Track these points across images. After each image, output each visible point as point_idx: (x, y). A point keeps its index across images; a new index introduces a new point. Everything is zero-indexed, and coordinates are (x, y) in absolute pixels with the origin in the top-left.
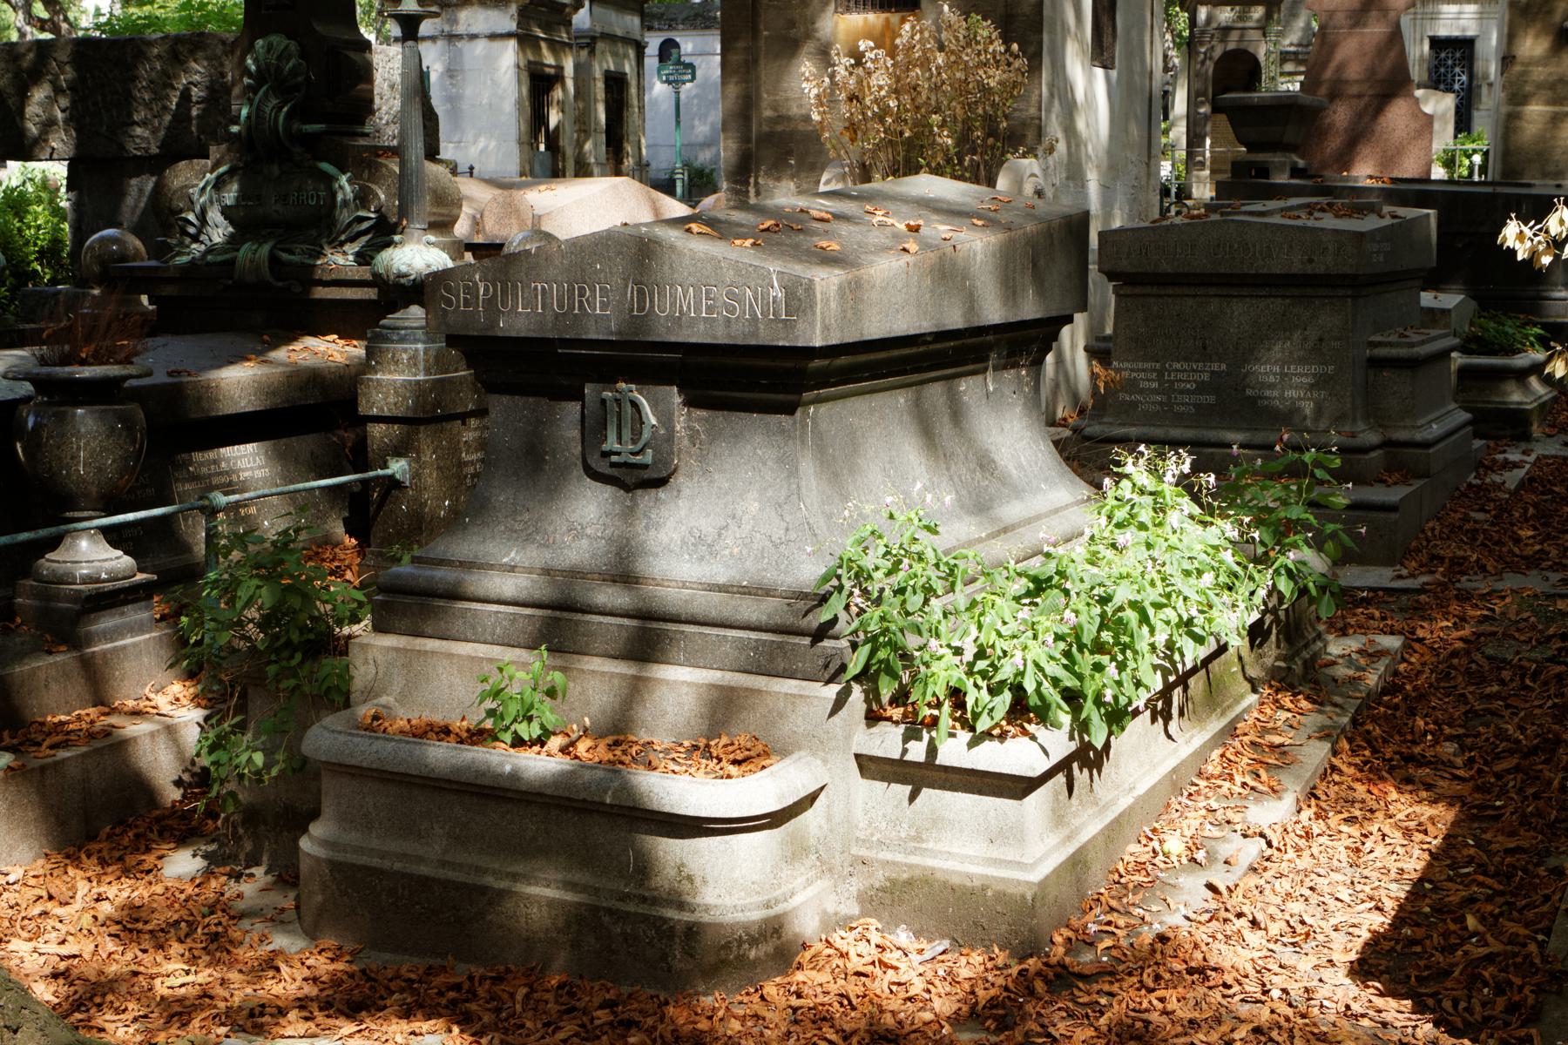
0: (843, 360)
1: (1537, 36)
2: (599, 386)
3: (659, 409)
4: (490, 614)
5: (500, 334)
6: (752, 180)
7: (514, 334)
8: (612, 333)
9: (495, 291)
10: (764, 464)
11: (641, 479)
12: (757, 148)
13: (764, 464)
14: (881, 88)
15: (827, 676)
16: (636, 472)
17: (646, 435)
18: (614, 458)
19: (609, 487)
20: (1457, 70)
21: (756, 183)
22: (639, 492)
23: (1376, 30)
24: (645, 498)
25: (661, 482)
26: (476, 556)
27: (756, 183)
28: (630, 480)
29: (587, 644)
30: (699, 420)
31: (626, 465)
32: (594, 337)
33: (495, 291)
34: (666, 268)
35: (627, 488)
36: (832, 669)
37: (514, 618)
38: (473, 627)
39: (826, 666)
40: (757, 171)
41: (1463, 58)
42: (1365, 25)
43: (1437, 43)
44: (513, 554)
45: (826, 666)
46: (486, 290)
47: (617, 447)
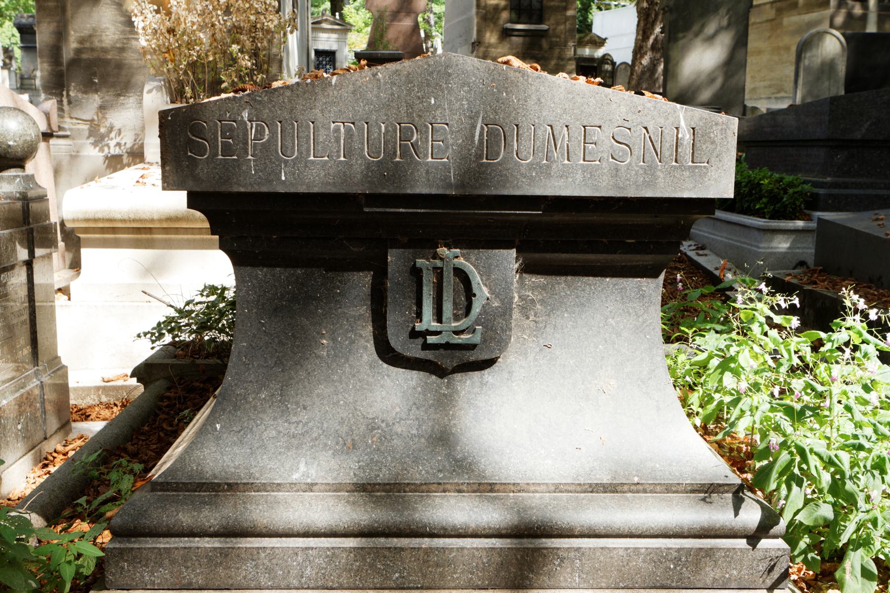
0: (101, 225)
1: (492, 32)
2: (408, 253)
3: (495, 273)
4: (295, 552)
5: (281, 189)
6: (65, 93)
7: (302, 189)
8: (450, 186)
9: (273, 133)
10: (619, 335)
11: (455, 361)
12: (68, 69)
13: (619, 335)
14: (193, 23)
15: (769, 583)
16: (458, 353)
17: (476, 309)
18: (431, 339)
19: (415, 373)
20: (328, 67)
21: (68, 95)
22: (458, 376)
23: (406, 23)
24: (468, 385)
25: (489, 363)
26: (251, 475)
27: (68, 95)
28: (448, 364)
29: (442, 576)
30: (533, 288)
31: (448, 346)
32: (425, 191)
33: (273, 133)
34: (531, 102)
35: (440, 372)
36: (776, 575)
37: (333, 554)
38: (269, 570)
39: (771, 569)
40: (69, 86)
41: (330, 61)
42: (400, 21)
43: (318, 53)
44: (302, 468)
45: (771, 569)
46: (260, 132)
47: (435, 326)
